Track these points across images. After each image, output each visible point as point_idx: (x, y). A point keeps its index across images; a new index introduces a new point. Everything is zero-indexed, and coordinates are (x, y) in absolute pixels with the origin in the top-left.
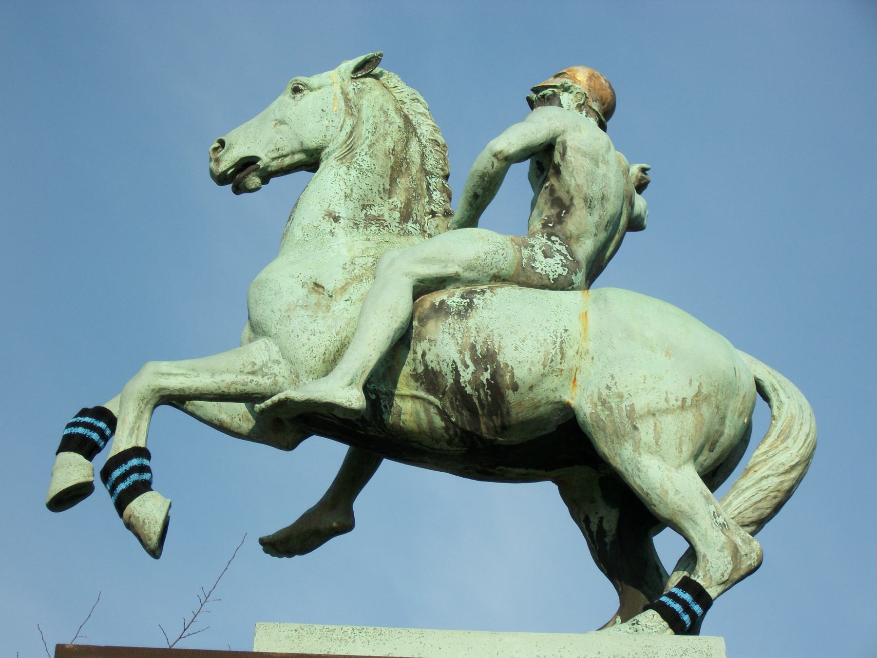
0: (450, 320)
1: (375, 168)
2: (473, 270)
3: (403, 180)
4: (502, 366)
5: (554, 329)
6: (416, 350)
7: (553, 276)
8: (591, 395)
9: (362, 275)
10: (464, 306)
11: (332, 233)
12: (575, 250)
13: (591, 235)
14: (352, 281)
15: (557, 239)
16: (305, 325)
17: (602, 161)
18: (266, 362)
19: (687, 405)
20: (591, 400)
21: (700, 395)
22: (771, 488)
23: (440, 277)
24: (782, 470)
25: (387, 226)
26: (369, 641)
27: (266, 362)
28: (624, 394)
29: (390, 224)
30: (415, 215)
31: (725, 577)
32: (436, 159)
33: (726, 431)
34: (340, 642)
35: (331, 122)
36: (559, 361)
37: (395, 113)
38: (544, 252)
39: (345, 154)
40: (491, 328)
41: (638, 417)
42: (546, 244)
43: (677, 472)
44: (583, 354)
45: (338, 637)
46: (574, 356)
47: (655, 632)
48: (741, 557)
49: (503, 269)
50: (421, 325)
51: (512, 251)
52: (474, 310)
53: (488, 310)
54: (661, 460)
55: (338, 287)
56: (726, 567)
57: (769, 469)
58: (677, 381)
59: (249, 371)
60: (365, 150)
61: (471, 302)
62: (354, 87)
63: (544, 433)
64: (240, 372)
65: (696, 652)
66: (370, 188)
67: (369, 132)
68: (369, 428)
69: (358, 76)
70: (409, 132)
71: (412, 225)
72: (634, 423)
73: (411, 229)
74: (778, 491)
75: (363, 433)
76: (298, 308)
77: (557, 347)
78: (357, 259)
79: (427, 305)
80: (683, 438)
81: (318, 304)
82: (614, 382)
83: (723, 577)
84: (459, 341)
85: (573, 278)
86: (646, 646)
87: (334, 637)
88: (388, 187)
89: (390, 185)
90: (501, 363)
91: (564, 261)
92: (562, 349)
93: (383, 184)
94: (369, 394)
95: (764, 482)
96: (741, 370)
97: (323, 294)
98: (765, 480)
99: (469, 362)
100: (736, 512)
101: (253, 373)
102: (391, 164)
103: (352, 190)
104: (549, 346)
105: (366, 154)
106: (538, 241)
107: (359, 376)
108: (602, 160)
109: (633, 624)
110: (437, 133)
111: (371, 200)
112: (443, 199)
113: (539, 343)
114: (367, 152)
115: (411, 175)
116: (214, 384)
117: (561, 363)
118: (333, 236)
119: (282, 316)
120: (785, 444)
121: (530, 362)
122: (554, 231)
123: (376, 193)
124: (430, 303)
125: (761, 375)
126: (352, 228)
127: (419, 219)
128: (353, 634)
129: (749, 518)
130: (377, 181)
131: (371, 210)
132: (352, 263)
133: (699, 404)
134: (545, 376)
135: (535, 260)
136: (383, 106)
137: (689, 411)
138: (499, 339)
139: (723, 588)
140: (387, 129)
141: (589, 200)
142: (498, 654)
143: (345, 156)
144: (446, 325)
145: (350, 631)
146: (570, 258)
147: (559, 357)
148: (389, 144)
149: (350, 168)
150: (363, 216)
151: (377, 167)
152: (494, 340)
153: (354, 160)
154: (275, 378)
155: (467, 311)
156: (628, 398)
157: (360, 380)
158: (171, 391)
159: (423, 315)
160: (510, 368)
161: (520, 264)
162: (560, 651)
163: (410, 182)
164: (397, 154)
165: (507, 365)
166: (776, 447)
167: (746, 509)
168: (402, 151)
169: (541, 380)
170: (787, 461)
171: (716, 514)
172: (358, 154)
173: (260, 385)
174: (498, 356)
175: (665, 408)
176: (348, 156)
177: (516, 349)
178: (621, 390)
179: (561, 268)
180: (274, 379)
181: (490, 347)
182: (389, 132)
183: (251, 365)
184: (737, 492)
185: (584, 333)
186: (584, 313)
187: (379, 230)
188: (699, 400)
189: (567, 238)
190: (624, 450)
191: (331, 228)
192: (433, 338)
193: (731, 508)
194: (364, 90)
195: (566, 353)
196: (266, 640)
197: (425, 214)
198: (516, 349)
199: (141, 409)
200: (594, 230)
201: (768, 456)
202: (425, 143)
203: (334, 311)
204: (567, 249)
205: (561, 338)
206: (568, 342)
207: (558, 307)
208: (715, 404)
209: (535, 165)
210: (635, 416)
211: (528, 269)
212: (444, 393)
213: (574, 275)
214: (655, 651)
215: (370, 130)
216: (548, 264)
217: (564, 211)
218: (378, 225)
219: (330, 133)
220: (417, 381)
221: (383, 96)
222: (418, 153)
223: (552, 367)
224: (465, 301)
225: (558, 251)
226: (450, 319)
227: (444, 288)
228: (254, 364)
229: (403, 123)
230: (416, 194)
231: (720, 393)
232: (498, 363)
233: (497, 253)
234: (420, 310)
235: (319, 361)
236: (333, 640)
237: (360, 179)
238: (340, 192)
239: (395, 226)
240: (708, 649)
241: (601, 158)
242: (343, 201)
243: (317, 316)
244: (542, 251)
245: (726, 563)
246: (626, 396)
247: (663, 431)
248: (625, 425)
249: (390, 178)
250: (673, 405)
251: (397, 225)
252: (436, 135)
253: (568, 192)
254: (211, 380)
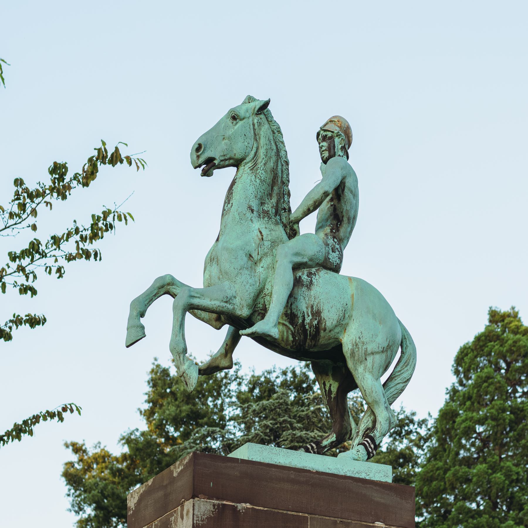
8: (352, 340)
20: (352, 342)
38: (332, 249)
63: (327, 349)
87: (273, 452)
88: (270, 192)
95: (398, 386)
99: (310, 314)
101: (226, 302)
116: (211, 306)
120: (406, 368)
169: (334, 328)
190: (360, 368)
212: (296, 325)
220: (286, 317)
228: (227, 297)
232: (321, 317)
246: (365, 343)
253: (342, 212)
254: (210, 303)
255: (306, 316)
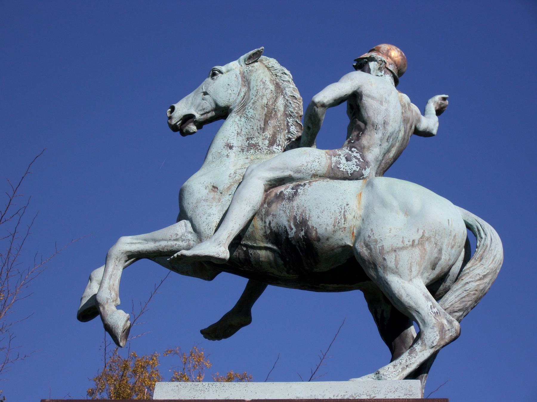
0: (284, 203)
1: (255, 116)
2: (300, 173)
3: (272, 122)
4: (310, 227)
5: (341, 204)
6: (266, 221)
7: (350, 172)
9: (240, 179)
10: (292, 194)
11: (227, 156)
12: (366, 155)
13: (377, 145)
14: (234, 183)
15: (355, 149)
16: (205, 210)
17: (385, 101)
18: (184, 233)
19: (415, 243)
21: (424, 238)
22: (471, 289)
23: (280, 178)
24: (478, 278)
25: (260, 149)
26: (217, 391)
27: (184, 233)
28: (378, 240)
29: (262, 148)
30: (278, 141)
31: (434, 344)
32: (293, 107)
33: (443, 257)
34: (201, 391)
35: (233, 91)
36: (343, 222)
37: (270, 82)
38: (346, 158)
39: (240, 109)
40: (305, 206)
41: (386, 252)
42: (347, 154)
43: (409, 283)
44: (358, 218)
45: (200, 388)
46: (352, 219)
47: (389, 378)
48: (446, 331)
49: (319, 170)
50: (268, 207)
51: (325, 159)
52: (297, 196)
53: (304, 196)
54: (399, 277)
55: (225, 187)
56: (435, 338)
57: (470, 278)
58: (410, 230)
59: (174, 239)
60: (251, 106)
61: (297, 191)
62: (247, 70)
64: (169, 239)
65: (403, 389)
66: (252, 127)
67: (253, 95)
68: (245, 267)
69: (250, 62)
70: (278, 93)
71: (276, 147)
72: (384, 256)
73: (275, 150)
74: (476, 290)
75: (242, 269)
76: (202, 201)
77: (342, 215)
78: (238, 170)
79: (273, 194)
80: (413, 264)
81: (214, 198)
82: (372, 233)
83: (433, 344)
84: (288, 215)
85: (363, 172)
86: (374, 387)
87: (198, 389)
88: (263, 126)
89: (264, 125)
90: (310, 226)
91: (358, 162)
92: (344, 215)
93: (260, 125)
94: (243, 247)
96: (453, 220)
97: (217, 192)
98: (468, 284)
99: (293, 226)
100: (450, 304)
101: (177, 240)
102: (265, 113)
103: (241, 130)
104: (337, 214)
105: (251, 108)
106: (343, 152)
107: (225, 240)
108: (385, 100)
109: (377, 374)
110: (295, 91)
111: (253, 134)
112: (296, 130)
113: (331, 213)
114: (251, 107)
115: (277, 118)
117: (344, 224)
118: (227, 158)
119: (193, 206)
120: (481, 263)
121: (326, 224)
122: (354, 145)
123: (255, 130)
124: (275, 193)
125: (471, 222)
126: (240, 152)
127: (281, 143)
128: (208, 387)
129: (457, 307)
130: (256, 123)
131: (252, 140)
132: (235, 173)
133: (423, 243)
134: (335, 232)
135: (340, 163)
136: (262, 79)
137: (417, 247)
138: (309, 212)
139: (434, 350)
140: (264, 92)
141: (375, 125)
142: (288, 395)
143: (240, 110)
144: (281, 206)
145: (207, 385)
146: (362, 160)
147: (343, 220)
148: (265, 101)
149: (242, 117)
150: (247, 144)
151: (256, 115)
152: (306, 213)
153: (244, 112)
154: (189, 242)
155: (293, 197)
156: (380, 242)
157: (226, 242)
158: (133, 253)
159: (270, 201)
160: (315, 229)
161: (330, 166)
162: (324, 392)
163: (276, 122)
164: (269, 107)
165: (313, 227)
166: (476, 265)
167: (456, 302)
168: (272, 105)
170: (481, 272)
171: (432, 307)
172: (247, 108)
173: (181, 246)
174: (308, 222)
175: (402, 247)
176: (241, 110)
177: (318, 217)
178: (376, 238)
179: (355, 167)
180: (188, 242)
181: (304, 217)
182: (265, 94)
183: (175, 236)
184: (451, 292)
185: (359, 205)
186: (360, 194)
187: (255, 152)
188: (423, 241)
189: (362, 148)
191: (227, 153)
192: (275, 214)
193: (447, 302)
194: (253, 70)
195: (347, 218)
196: (161, 392)
197: (285, 140)
198: (318, 217)
199: (116, 264)
200: (379, 143)
201: (470, 270)
202: (287, 98)
203: (222, 201)
204: (360, 155)
205: (344, 209)
206: (349, 211)
207: (345, 191)
208: (434, 242)
209: (349, 106)
210: (384, 252)
211: (335, 169)
213: (364, 170)
214: (379, 389)
215: (254, 94)
216: (348, 165)
217: (361, 133)
218: (255, 149)
219: (232, 97)
221: (263, 73)
222: (283, 104)
223: (339, 226)
224: (293, 191)
225: (355, 157)
226: (284, 202)
227: (284, 184)
228: (177, 235)
229: (274, 88)
230: (279, 129)
231: (437, 235)
232: (308, 226)
233: (314, 161)
234: (269, 197)
235: (213, 231)
236: (197, 391)
237: (246, 123)
238: (234, 131)
239: (265, 149)
240: (410, 387)
241: (384, 100)
242: (236, 136)
243: (213, 205)
244: (345, 158)
245: (435, 335)
246: (379, 241)
247: (400, 260)
248: (379, 258)
249: (264, 121)
250: (407, 245)
251: (266, 148)
252: (294, 93)
255: (289, 231)
